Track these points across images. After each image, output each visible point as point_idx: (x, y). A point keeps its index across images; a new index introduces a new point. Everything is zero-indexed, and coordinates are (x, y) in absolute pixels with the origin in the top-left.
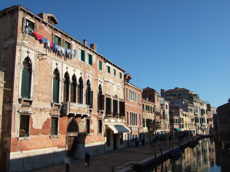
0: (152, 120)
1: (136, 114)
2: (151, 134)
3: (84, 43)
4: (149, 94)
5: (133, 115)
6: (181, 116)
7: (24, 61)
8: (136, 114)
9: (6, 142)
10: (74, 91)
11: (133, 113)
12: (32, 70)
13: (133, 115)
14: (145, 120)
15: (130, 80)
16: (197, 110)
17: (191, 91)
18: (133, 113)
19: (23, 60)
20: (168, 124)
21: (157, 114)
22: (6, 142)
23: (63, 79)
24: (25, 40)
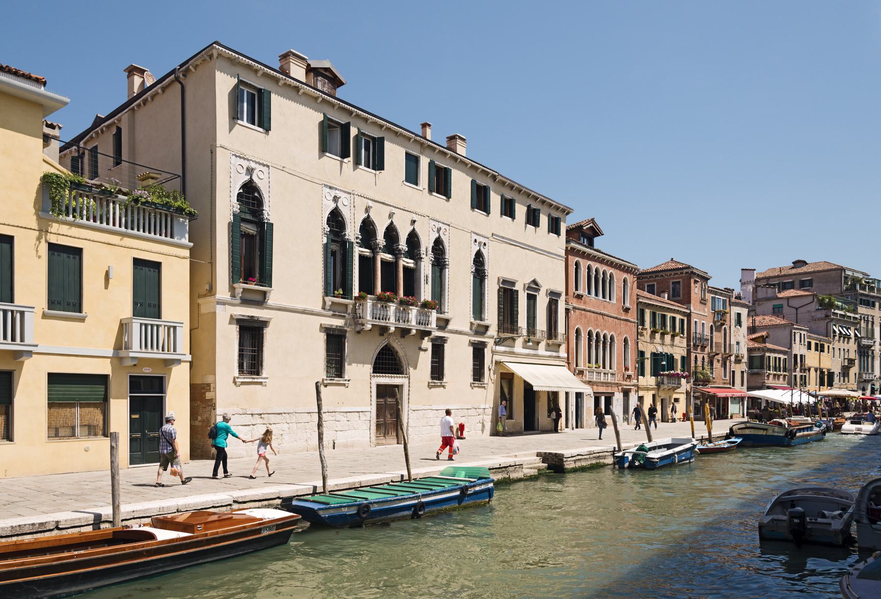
0: (678, 357)
1: (612, 338)
2: (670, 397)
3: (425, 133)
4: (671, 281)
5: (597, 341)
6: (798, 349)
7: (239, 195)
8: (612, 338)
9: (209, 385)
10: (534, 317)
11: (598, 335)
12: (262, 214)
13: (604, 343)
14: (648, 355)
15: (596, 240)
16: (873, 330)
17: (850, 270)
18: (598, 335)
19: (236, 190)
20: (742, 372)
21: (696, 343)
22: (209, 385)
23: (357, 238)
24: (420, 313)
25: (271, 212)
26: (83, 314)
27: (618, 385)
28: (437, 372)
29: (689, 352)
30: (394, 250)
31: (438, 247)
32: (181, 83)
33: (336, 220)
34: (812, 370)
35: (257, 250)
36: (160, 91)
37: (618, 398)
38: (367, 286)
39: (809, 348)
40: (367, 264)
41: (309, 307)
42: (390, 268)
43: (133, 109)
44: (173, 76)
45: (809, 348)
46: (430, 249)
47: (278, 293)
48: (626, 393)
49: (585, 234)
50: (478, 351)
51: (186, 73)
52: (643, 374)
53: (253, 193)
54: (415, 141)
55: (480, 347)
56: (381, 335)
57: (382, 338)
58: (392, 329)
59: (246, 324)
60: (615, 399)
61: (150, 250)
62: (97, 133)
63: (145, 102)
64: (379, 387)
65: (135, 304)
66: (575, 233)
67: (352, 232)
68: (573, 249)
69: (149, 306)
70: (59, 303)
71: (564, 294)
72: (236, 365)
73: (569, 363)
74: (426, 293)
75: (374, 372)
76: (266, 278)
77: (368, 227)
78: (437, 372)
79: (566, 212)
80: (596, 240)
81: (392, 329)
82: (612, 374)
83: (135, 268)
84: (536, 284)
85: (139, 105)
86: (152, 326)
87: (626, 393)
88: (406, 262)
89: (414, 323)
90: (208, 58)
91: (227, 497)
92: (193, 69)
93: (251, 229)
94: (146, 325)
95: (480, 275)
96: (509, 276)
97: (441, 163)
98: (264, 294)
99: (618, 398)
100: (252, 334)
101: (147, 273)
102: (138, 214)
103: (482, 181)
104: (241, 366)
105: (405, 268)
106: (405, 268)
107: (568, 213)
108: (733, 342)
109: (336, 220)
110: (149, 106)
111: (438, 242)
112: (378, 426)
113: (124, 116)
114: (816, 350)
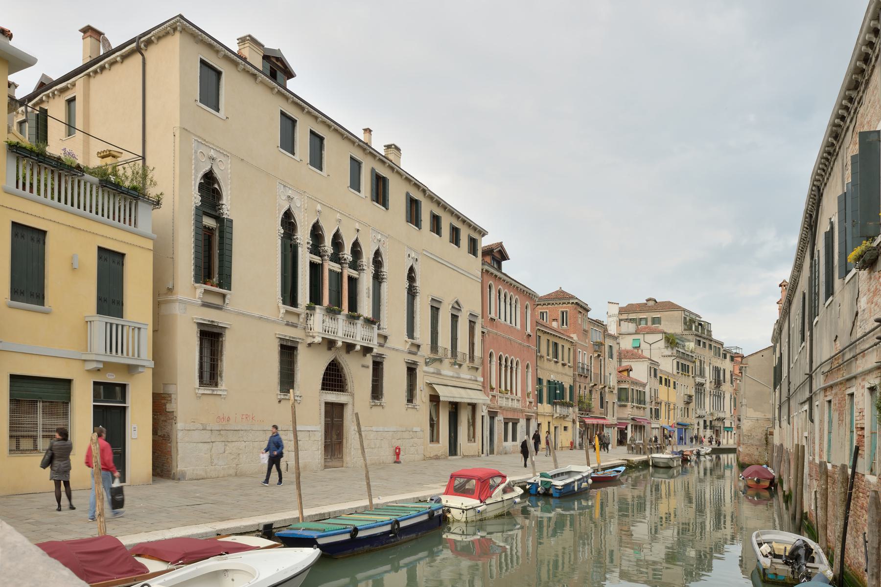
0: (567, 386)
15: (504, 263)
21: (583, 374)
25: (229, 207)
26: (46, 307)
27: (522, 411)
28: (377, 392)
29: (574, 381)
30: (340, 259)
31: (378, 262)
32: (142, 55)
33: (288, 222)
34: (663, 404)
35: (217, 248)
36: (118, 59)
37: (522, 423)
38: (316, 297)
39: (661, 382)
40: (315, 269)
41: (265, 315)
42: (337, 277)
43: (88, 75)
44: (134, 45)
45: (661, 382)
46: (371, 260)
47: (237, 295)
48: (528, 420)
49: (497, 255)
50: (411, 371)
51: (149, 43)
52: (541, 401)
53: (213, 184)
54: (359, 145)
55: (413, 366)
56: (330, 349)
57: (330, 353)
58: (340, 344)
59: (206, 329)
60: (519, 426)
61: (115, 238)
62: (48, 96)
63: (103, 68)
64: (327, 404)
65: (99, 299)
66: (488, 252)
67: (303, 236)
68: (487, 271)
69: (113, 302)
70: (22, 293)
71: (480, 317)
72: (197, 374)
73: (484, 387)
74: (365, 308)
75: (323, 389)
76: (225, 281)
77: (316, 233)
78: (377, 392)
79: (483, 233)
80: (504, 263)
81: (340, 344)
82: (518, 400)
83: (100, 258)
84: (459, 305)
85: (95, 72)
86: (117, 325)
87: (528, 420)
88: (348, 272)
89: (358, 338)
90: (172, 31)
91: (210, 530)
92: (155, 41)
93: (209, 222)
94: (111, 324)
95: (412, 293)
96: (437, 295)
97: (383, 172)
98: (224, 296)
99: (522, 423)
100: (211, 338)
101: (111, 263)
102: (79, 186)
103: (417, 195)
104: (201, 377)
105: (330, 271)
106: (330, 271)
107: (483, 235)
108: (607, 374)
109: (288, 222)
110: (106, 73)
111: (377, 253)
112: (326, 447)
113: (79, 80)
114: (666, 384)
